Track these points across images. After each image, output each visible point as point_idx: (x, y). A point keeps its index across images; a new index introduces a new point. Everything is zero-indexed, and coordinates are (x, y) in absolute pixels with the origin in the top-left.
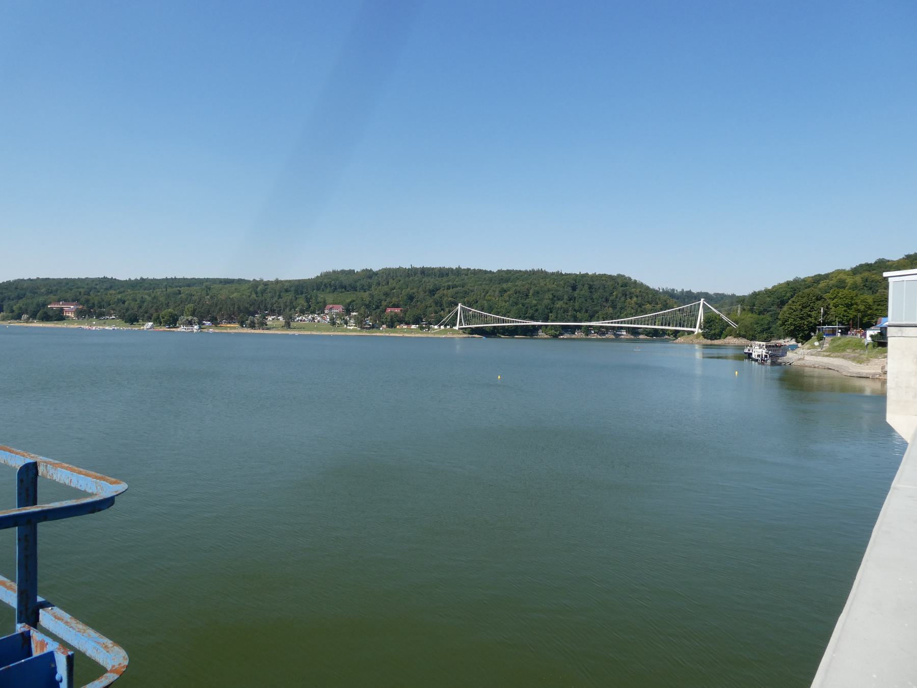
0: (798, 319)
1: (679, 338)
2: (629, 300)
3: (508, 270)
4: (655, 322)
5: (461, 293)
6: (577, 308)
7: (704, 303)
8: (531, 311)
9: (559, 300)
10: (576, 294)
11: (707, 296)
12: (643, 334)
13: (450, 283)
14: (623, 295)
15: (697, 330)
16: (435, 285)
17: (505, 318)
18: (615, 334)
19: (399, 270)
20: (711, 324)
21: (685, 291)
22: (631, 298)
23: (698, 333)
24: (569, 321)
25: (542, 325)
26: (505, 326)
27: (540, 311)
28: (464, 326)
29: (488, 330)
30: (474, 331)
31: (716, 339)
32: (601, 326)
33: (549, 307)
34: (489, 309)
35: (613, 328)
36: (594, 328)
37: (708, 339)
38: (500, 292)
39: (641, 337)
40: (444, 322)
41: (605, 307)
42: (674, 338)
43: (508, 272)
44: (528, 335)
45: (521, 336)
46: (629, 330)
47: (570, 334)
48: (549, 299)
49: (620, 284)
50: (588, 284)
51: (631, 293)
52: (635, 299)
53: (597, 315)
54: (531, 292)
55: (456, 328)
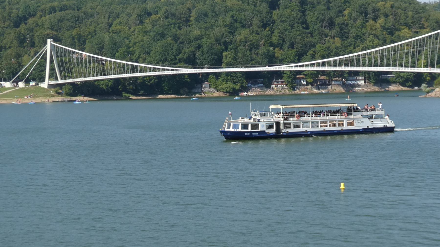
2: (371, 22)
5: (69, 20)
6: (275, 39)
8: (187, 50)
9: (243, 26)
12: (395, 83)
14: (361, 14)
18: (344, 85)
22: (375, 19)
24: (259, 64)
25: (208, 74)
26: (136, 78)
27: (205, 49)
28: (60, 81)
32: (318, 72)
33: (223, 40)
34: (112, 48)
35: (341, 74)
36: (305, 75)
38: (138, 16)
39: (393, 87)
40: (24, 74)
41: (326, 36)
45: (169, 96)
46: (367, 76)
47: (261, 88)
48: (226, 26)
51: (375, 10)
52: (381, 20)
53: (310, 52)
54: (194, 14)
55: (45, 85)
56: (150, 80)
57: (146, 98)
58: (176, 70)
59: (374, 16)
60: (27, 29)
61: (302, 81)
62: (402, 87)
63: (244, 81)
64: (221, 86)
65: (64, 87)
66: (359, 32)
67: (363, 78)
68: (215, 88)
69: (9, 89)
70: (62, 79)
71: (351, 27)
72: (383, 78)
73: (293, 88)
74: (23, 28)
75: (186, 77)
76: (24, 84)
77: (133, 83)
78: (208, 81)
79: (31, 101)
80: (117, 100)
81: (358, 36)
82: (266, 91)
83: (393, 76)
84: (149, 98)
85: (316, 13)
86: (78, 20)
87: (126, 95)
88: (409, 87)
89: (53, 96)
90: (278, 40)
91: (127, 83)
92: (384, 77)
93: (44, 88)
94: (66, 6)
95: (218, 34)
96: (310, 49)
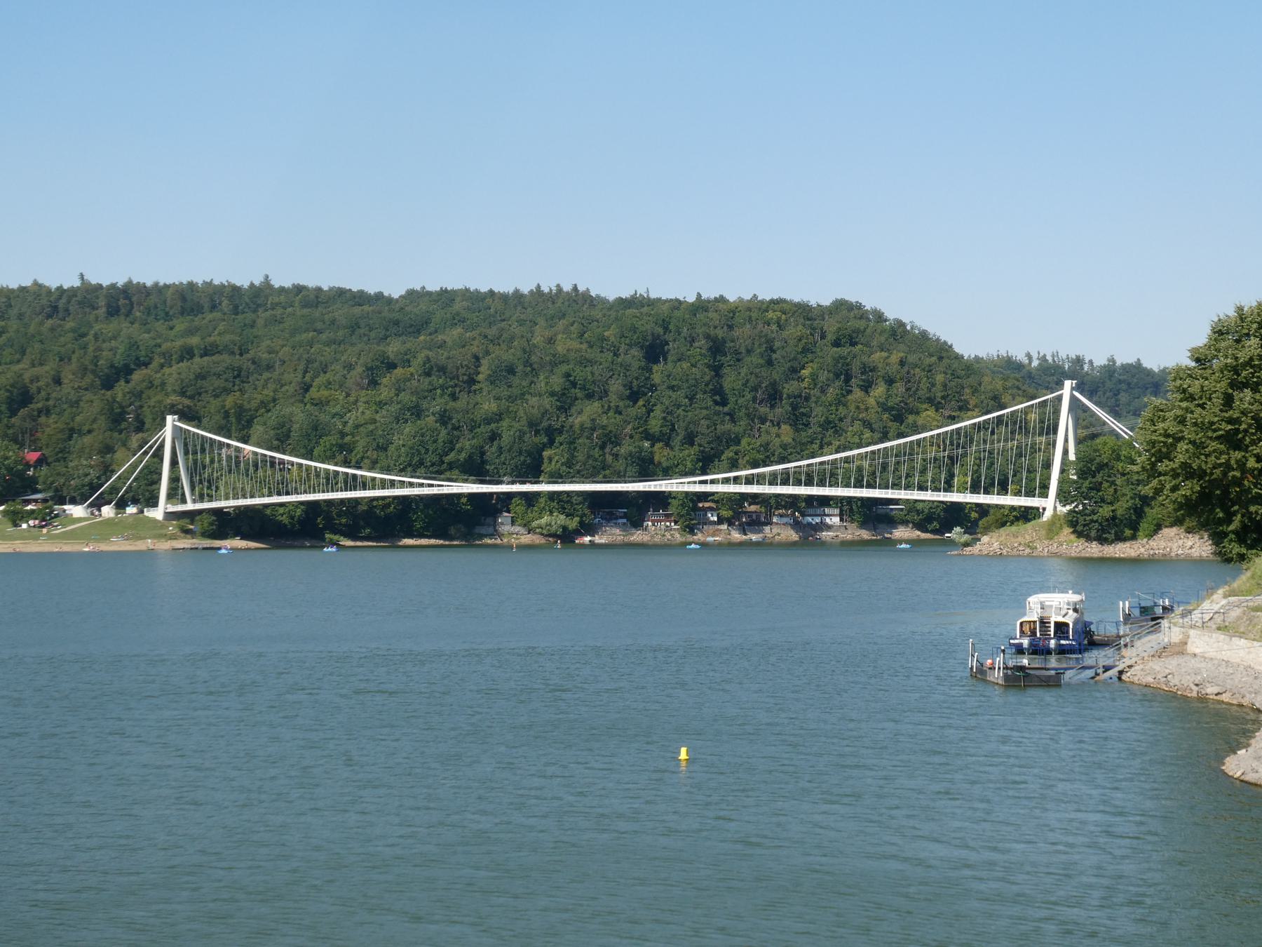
0: (1214, 445)
1: (985, 539)
2: (857, 394)
3: (444, 292)
4: (951, 476)
5: (219, 376)
6: (655, 425)
7: (1073, 398)
8: (467, 444)
9: (590, 396)
10: (658, 373)
11: (1076, 369)
12: (905, 522)
13: (194, 341)
14: (837, 376)
15: (1049, 505)
16: (134, 345)
17: (359, 472)
18: (797, 525)
19: (37, 292)
20: (1099, 478)
21: (1118, 363)
22: (866, 387)
23: (1055, 515)
25: (510, 496)
26: (357, 501)
27: (506, 438)
28: (190, 506)
29: (285, 519)
30: (224, 524)
31: (1120, 538)
32: (744, 496)
36: (717, 502)
37: (1089, 539)
38: (371, 369)
39: (900, 533)
40: (114, 489)
41: (763, 420)
42: (966, 537)
43: (446, 296)
44: (452, 531)
46: (848, 507)
48: (552, 394)
49: (830, 337)
50: (708, 337)
51: (867, 369)
52: (879, 390)
53: (729, 454)
54: (485, 370)
55: (157, 514)
56: (389, 505)
57: (375, 544)
58: (439, 486)
59: (864, 381)
60: (128, 393)
61: (710, 515)
62: (918, 533)
63: (587, 511)
64: (537, 522)
65: (198, 518)
66: (832, 414)
67: (837, 511)
68: (525, 525)
69: (80, 520)
70: (194, 501)
71: (816, 403)
72: (880, 512)
73: (691, 529)
74: (120, 390)
75: (464, 500)
76: (114, 511)
77: (346, 514)
78: (509, 512)
79: (117, 544)
80: (312, 547)
81: (830, 422)
82: (632, 535)
83: (902, 509)
84: (382, 544)
85: (744, 371)
86: (239, 376)
87: (332, 536)
88: (934, 532)
89: (173, 537)
90: (661, 427)
91: (334, 511)
92: (881, 509)
93: (155, 521)
94: (217, 346)
95: (535, 411)
96: (728, 448)
